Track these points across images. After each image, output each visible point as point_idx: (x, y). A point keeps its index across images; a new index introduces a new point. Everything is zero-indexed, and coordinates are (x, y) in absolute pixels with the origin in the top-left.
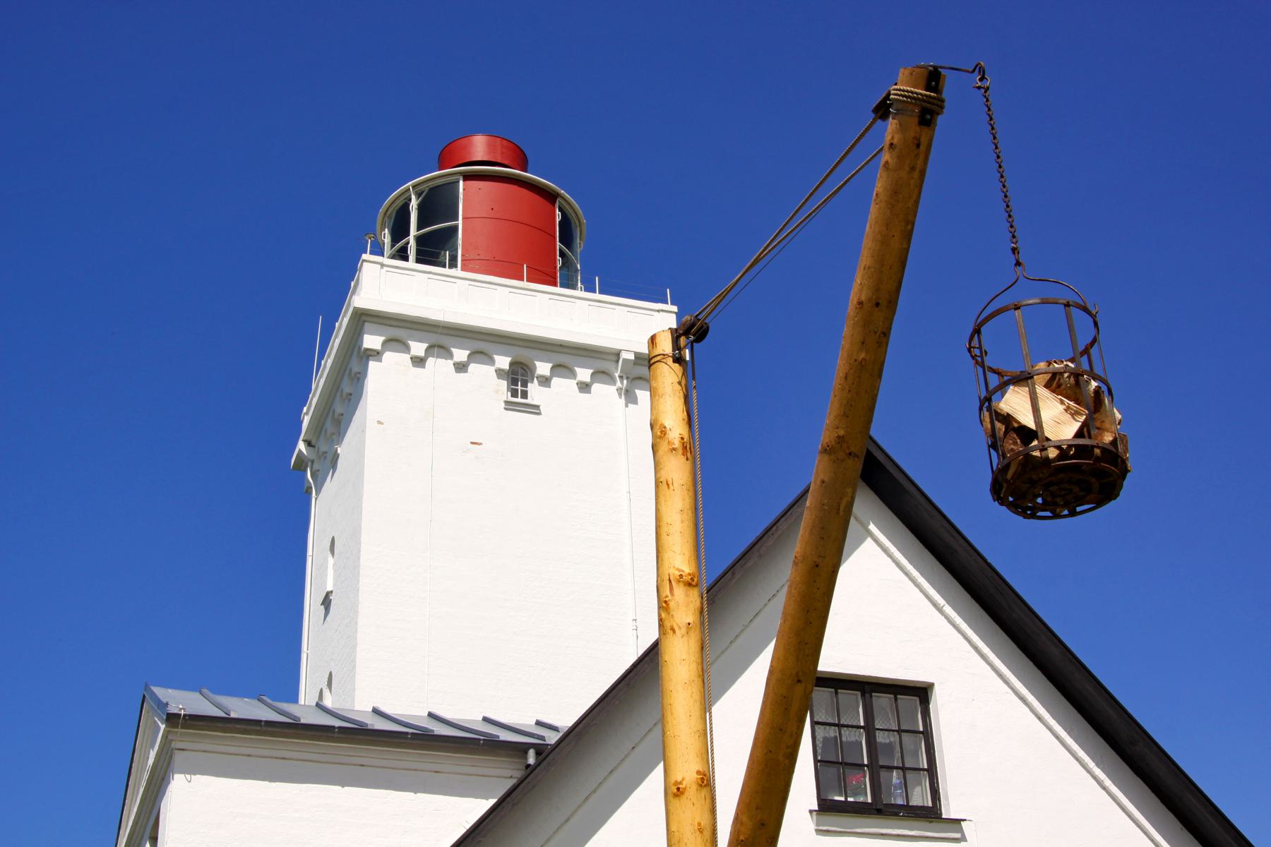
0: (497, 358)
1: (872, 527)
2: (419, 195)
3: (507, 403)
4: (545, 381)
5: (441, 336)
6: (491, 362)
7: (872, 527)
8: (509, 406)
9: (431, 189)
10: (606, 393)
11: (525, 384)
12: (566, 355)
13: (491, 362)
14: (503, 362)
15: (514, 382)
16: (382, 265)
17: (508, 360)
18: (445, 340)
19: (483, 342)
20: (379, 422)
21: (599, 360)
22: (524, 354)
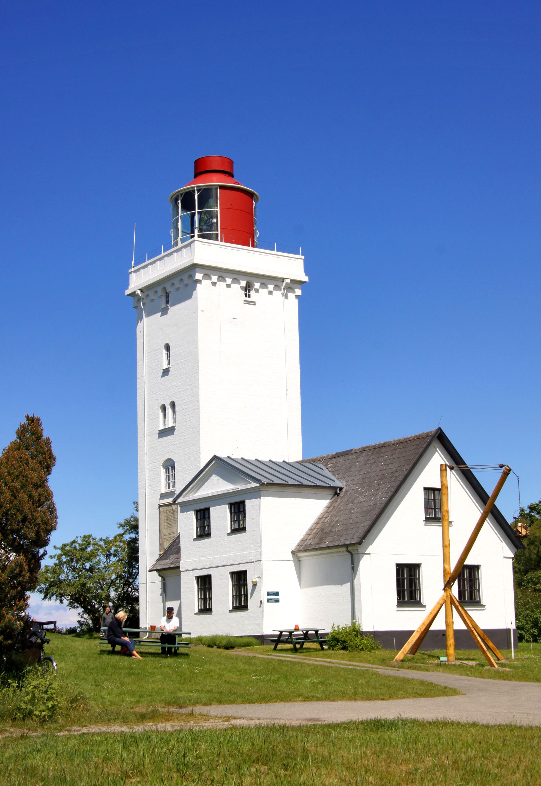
0: (241, 281)
1: (438, 450)
2: (198, 191)
3: (245, 301)
4: (257, 291)
5: (223, 273)
6: (239, 283)
7: (438, 450)
8: (246, 302)
9: (204, 189)
10: (277, 294)
11: (249, 292)
12: (266, 280)
13: (239, 283)
14: (243, 283)
15: (246, 291)
16: (201, 242)
17: (245, 282)
18: (224, 275)
19: (236, 275)
20: (202, 311)
21: (276, 281)
22: (250, 279)
